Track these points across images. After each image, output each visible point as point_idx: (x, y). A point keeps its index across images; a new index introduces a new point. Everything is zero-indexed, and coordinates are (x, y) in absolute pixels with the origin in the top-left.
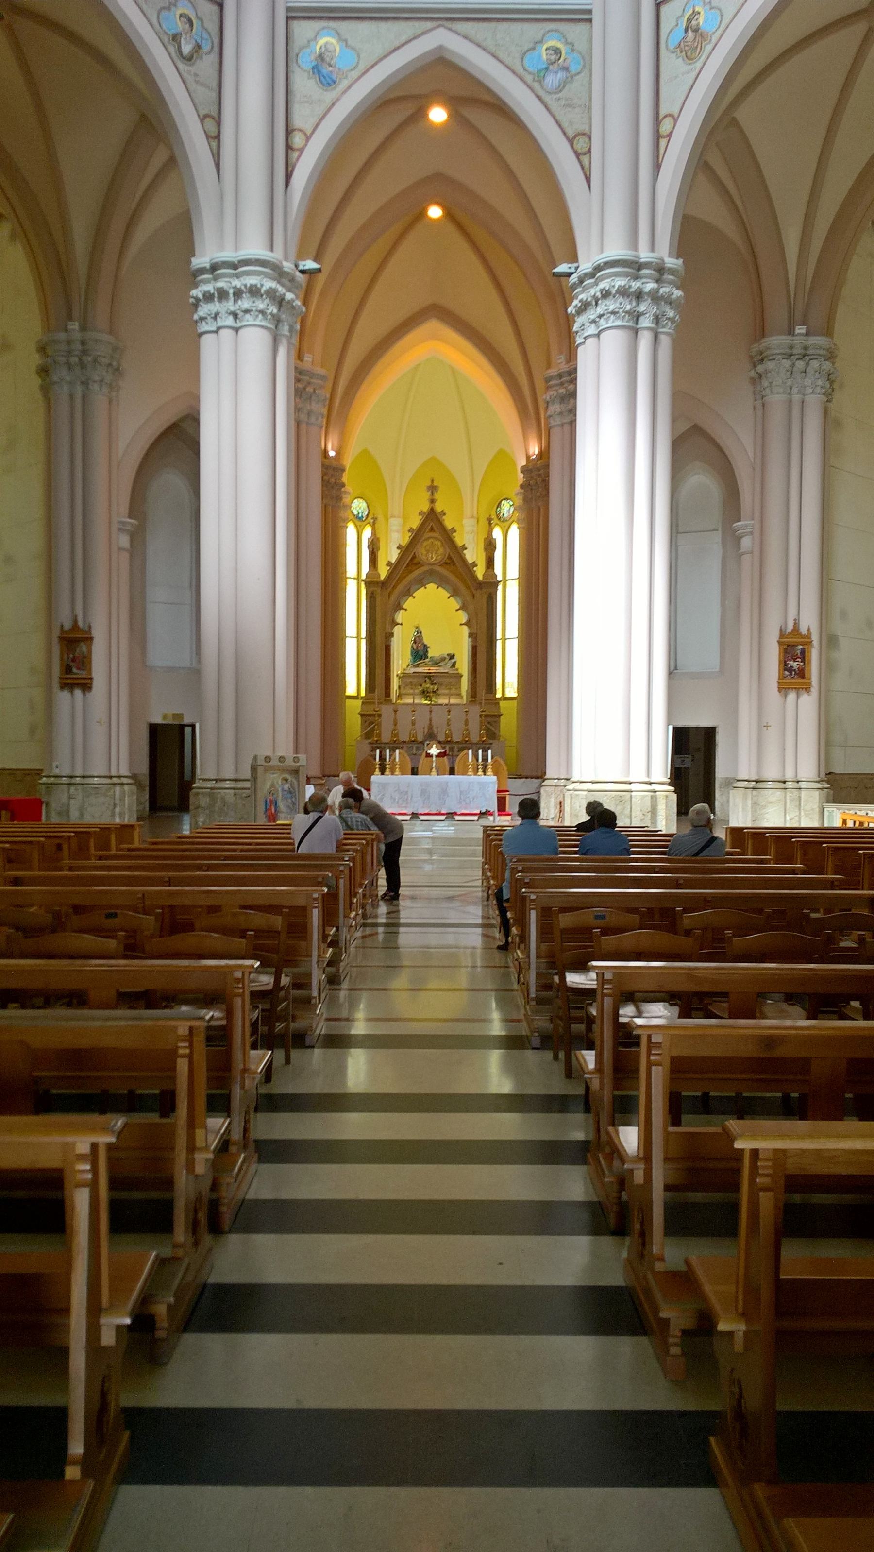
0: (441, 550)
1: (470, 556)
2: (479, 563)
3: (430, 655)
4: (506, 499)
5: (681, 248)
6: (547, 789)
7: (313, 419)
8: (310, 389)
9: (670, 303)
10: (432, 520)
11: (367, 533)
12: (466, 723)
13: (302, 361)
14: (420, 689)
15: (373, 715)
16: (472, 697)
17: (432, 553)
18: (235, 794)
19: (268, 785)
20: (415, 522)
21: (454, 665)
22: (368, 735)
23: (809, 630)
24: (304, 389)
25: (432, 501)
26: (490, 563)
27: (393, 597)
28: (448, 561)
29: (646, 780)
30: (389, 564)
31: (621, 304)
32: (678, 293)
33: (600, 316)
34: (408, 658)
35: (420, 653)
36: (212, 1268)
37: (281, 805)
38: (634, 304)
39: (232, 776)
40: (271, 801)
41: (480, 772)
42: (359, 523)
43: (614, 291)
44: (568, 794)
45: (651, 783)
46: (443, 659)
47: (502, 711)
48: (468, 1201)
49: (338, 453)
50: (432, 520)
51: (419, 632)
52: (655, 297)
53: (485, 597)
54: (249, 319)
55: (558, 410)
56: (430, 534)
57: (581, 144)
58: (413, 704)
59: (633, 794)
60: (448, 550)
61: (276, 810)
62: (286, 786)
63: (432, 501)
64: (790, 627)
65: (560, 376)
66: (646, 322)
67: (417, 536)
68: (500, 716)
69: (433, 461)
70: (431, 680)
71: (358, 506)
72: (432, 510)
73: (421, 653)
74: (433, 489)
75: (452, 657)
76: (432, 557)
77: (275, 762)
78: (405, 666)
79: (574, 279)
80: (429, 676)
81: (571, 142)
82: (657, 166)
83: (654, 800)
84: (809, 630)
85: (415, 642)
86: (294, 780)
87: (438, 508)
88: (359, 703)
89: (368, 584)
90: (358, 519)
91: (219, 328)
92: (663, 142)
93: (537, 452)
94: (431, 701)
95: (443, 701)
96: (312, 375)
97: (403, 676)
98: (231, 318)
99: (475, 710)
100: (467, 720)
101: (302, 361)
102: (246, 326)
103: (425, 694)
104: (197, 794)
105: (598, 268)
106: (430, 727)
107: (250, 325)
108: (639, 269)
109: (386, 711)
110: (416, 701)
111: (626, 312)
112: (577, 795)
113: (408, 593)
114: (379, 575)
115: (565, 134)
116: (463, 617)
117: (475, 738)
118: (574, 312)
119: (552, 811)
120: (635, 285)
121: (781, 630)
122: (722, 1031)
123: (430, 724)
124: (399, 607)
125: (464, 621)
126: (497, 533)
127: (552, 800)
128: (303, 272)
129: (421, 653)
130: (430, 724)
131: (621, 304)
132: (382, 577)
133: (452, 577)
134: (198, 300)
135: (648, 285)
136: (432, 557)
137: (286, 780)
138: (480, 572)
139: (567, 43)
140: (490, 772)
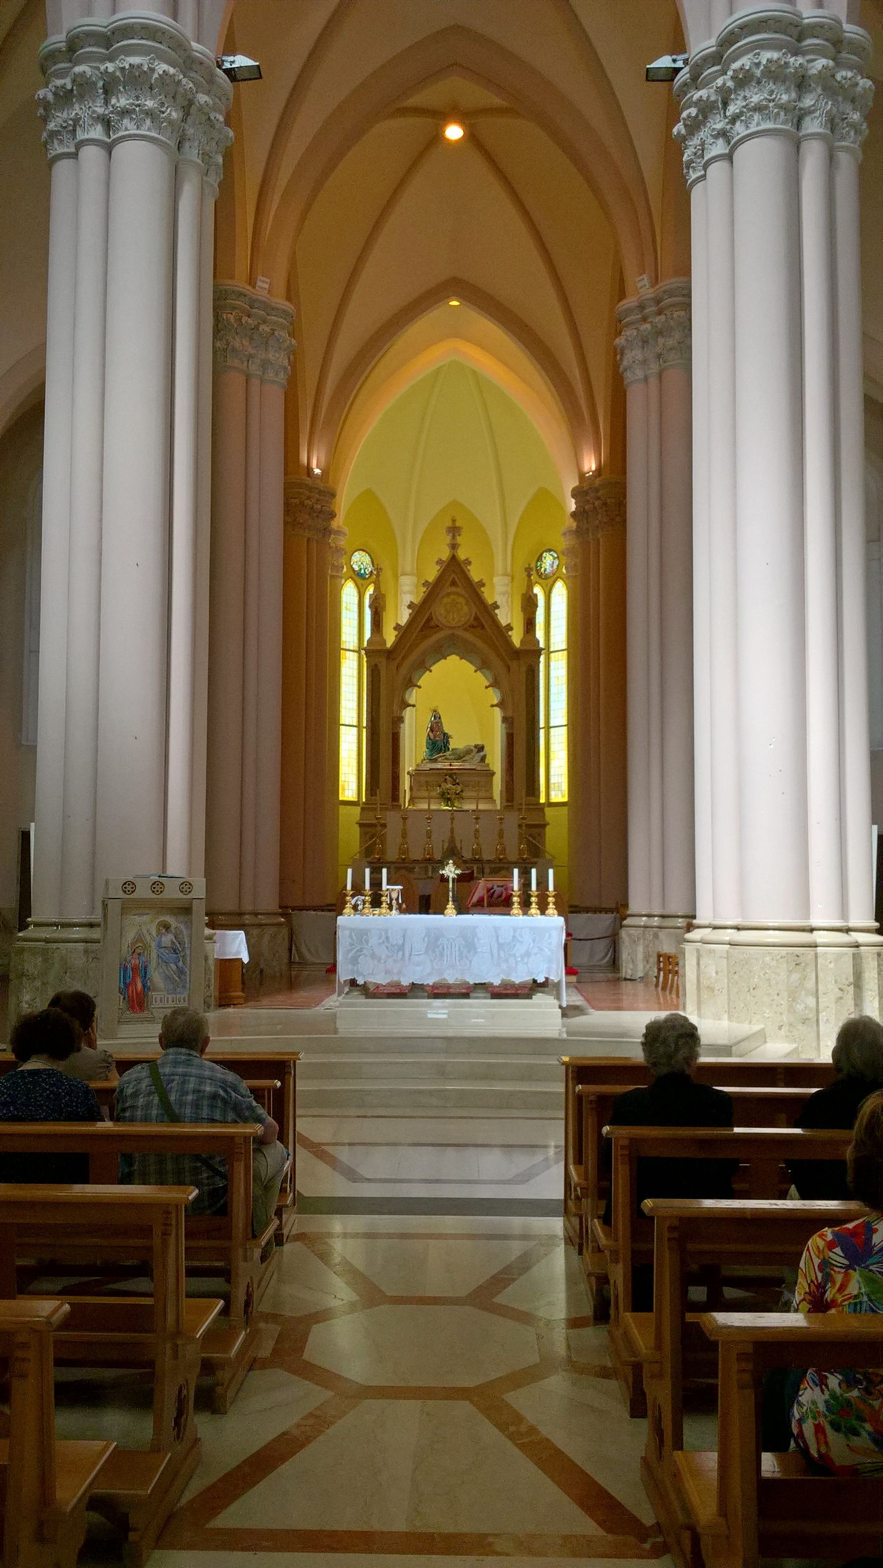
0: (466, 608)
1: (503, 617)
2: (514, 625)
3: (452, 746)
4: (550, 550)
6: (632, 931)
7: (270, 375)
8: (265, 328)
9: (853, 101)
10: (454, 571)
11: (371, 590)
12: (501, 835)
13: (254, 287)
14: (439, 790)
15: (374, 825)
16: (508, 801)
17: (453, 612)
18: (86, 951)
19: (130, 936)
20: (432, 574)
21: (483, 759)
22: (368, 851)
24: (256, 327)
25: (454, 546)
26: (530, 625)
27: (403, 671)
28: (475, 624)
29: (838, 923)
30: (397, 627)
31: (771, 92)
32: (865, 83)
33: (734, 120)
34: (423, 750)
35: (438, 743)
37: (156, 977)
38: (794, 95)
39: (83, 918)
40: (135, 969)
41: (534, 909)
42: (360, 581)
43: (758, 73)
44: (688, 947)
45: (848, 930)
46: (468, 752)
47: (548, 819)
49: (325, 472)
50: (454, 571)
51: (437, 717)
52: (830, 86)
53: (524, 669)
54: (128, 126)
55: (640, 357)
56: (454, 589)
58: (429, 810)
59: (818, 948)
60: (474, 610)
61: (144, 986)
62: (167, 939)
63: (454, 546)
65: (641, 307)
66: (813, 126)
67: (434, 591)
68: (544, 826)
69: (454, 504)
70: (452, 775)
71: (360, 560)
72: (453, 558)
73: (440, 744)
74: (454, 530)
75: (481, 748)
76: (455, 619)
77: (143, 892)
78: (419, 761)
79: (683, 76)
80: (451, 775)
83: (857, 960)
85: (432, 730)
86: (182, 927)
87: (462, 555)
88: (357, 810)
89: (369, 653)
90: (359, 578)
91: (80, 145)
93: (594, 468)
94: (452, 805)
95: (470, 806)
96: (269, 308)
97: (416, 775)
98: (99, 128)
99: (512, 820)
100: (501, 830)
101: (254, 287)
102: (123, 137)
103: (445, 797)
104: (22, 951)
105: (728, 40)
106: (452, 840)
107: (130, 136)
108: (800, 39)
109: (392, 819)
110: (433, 807)
111: (781, 107)
112: (711, 951)
113: (423, 666)
114: (384, 642)
116: (494, 696)
117: (513, 856)
118: (683, 131)
119: (640, 966)
120: (795, 61)
123: (452, 837)
124: (410, 683)
125: (496, 702)
126: (537, 590)
127: (640, 949)
128: (230, 73)
129: (440, 744)
130: (452, 837)
131: (771, 92)
132: (389, 644)
133: (479, 643)
134: (47, 106)
135: (818, 61)
136: (455, 619)
137: (167, 927)
138: (516, 637)
140: (551, 910)
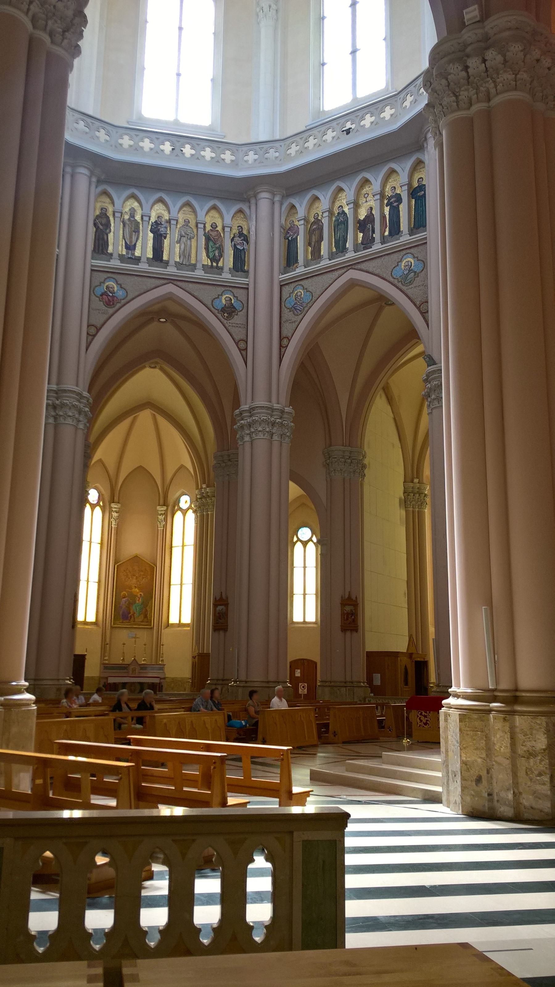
5: (293, 401)
23: (356, 598)
36: (432, 749)
48: (67, 961)
57: (242, 345)
64: (347, 596)
66: (275, 437)
81: (237, 344)
82: (281, 360)
84: (356, 598)
92: (283, 350)
115: (233, 339)
121: (342, 597)
122: (477, 694)
139: (234, 296)
